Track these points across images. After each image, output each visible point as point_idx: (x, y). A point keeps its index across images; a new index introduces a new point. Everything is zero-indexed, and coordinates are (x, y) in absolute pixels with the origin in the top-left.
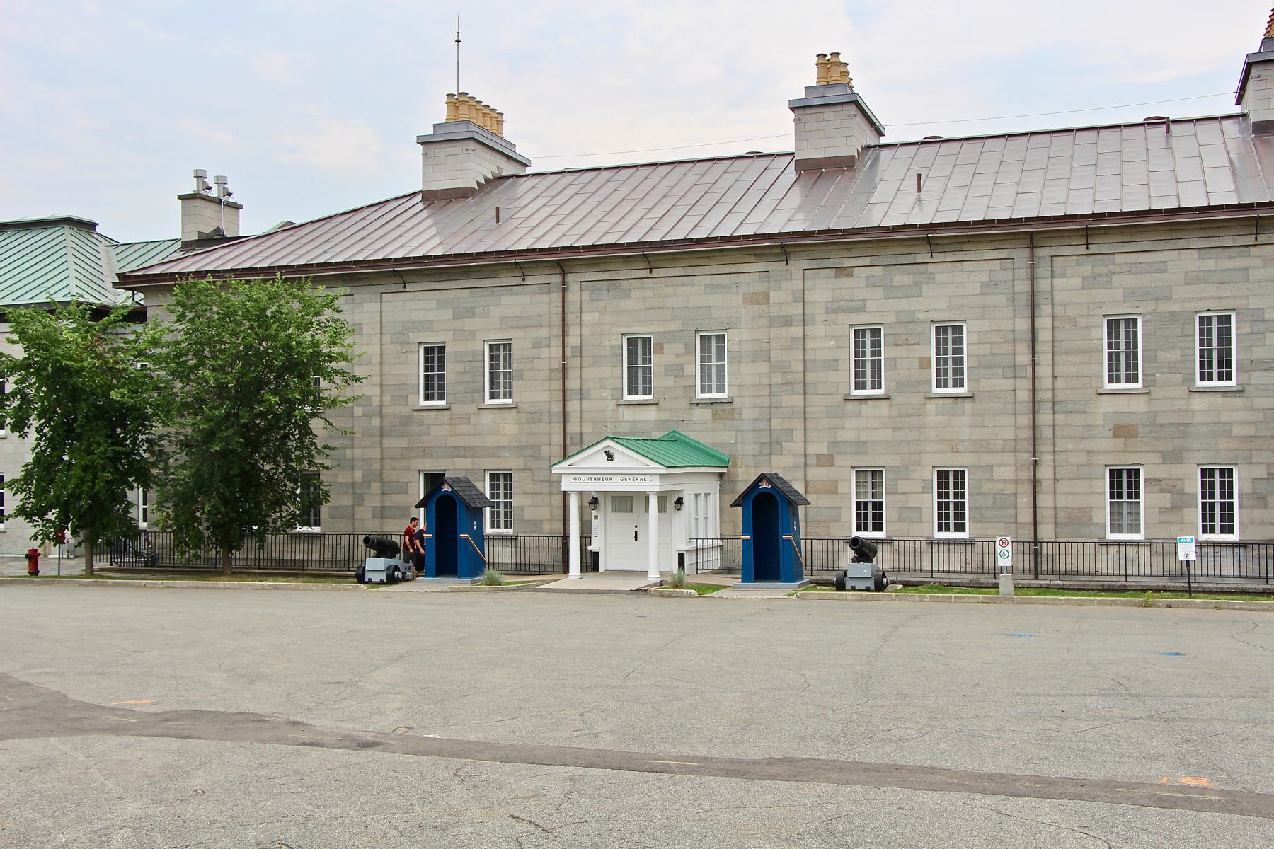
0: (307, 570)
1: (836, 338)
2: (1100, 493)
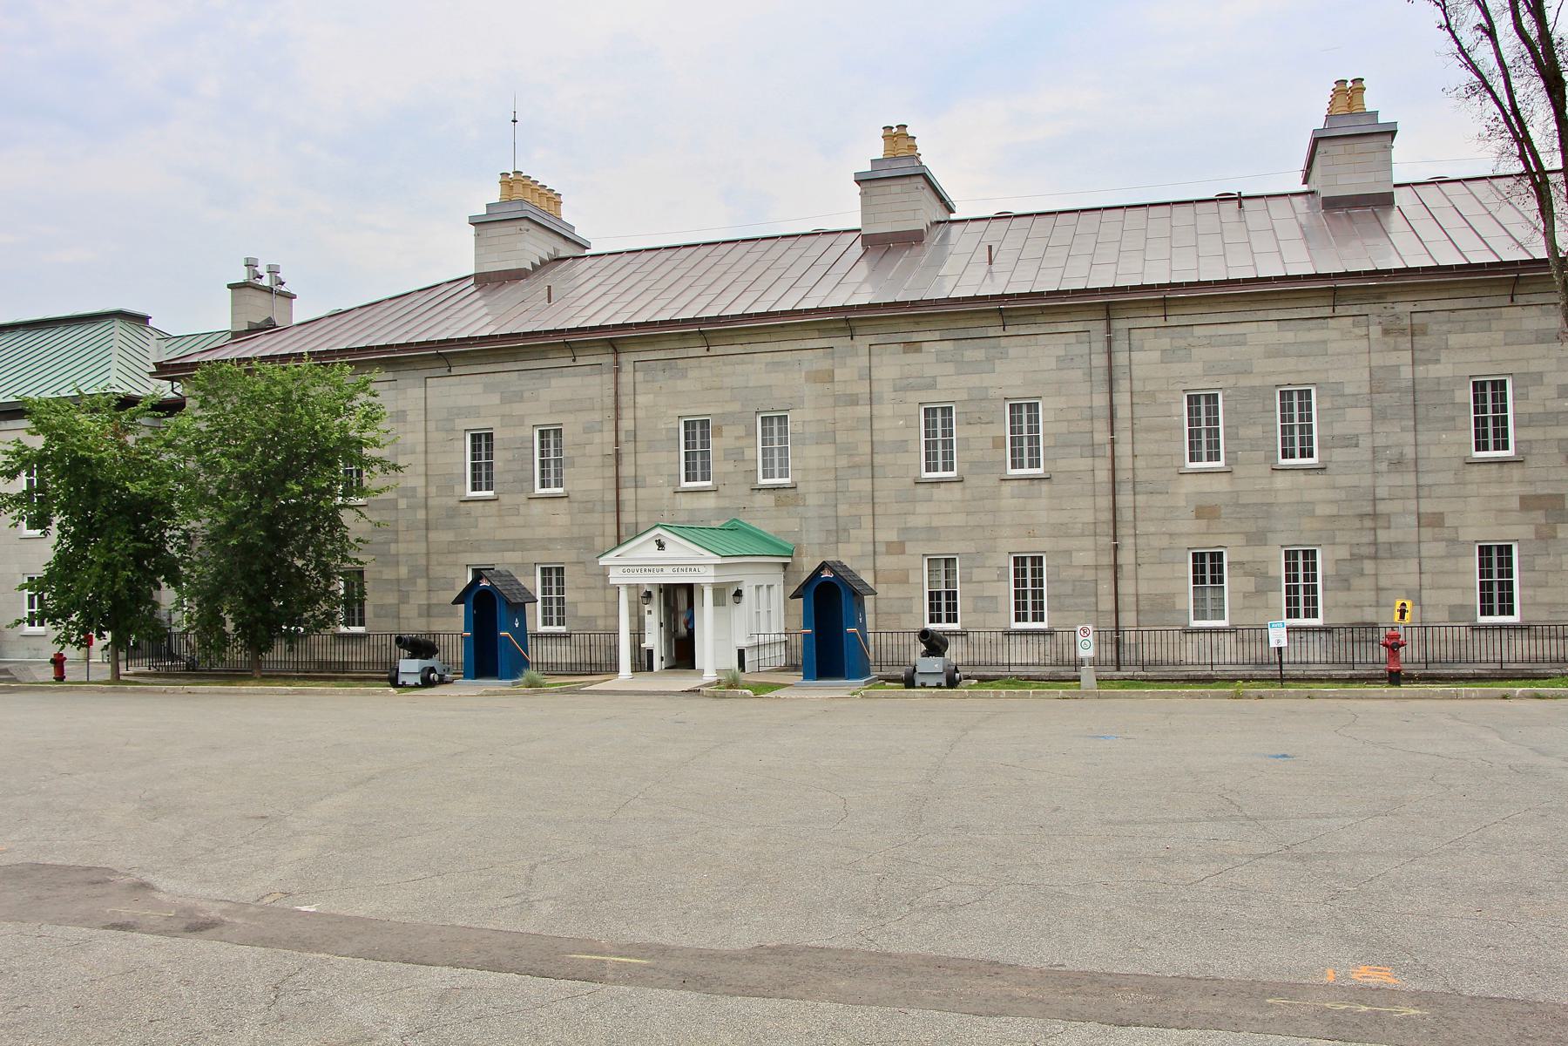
0: (347, 672)
2: (1183, 578)
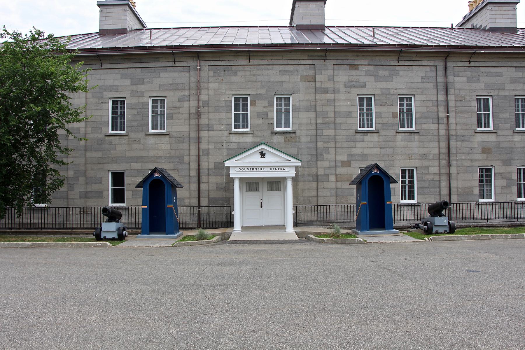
1: (350, 100)
